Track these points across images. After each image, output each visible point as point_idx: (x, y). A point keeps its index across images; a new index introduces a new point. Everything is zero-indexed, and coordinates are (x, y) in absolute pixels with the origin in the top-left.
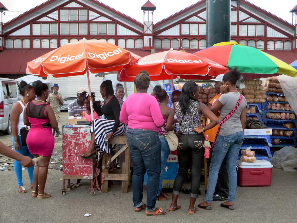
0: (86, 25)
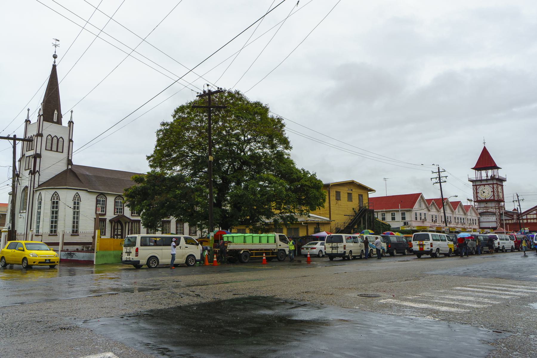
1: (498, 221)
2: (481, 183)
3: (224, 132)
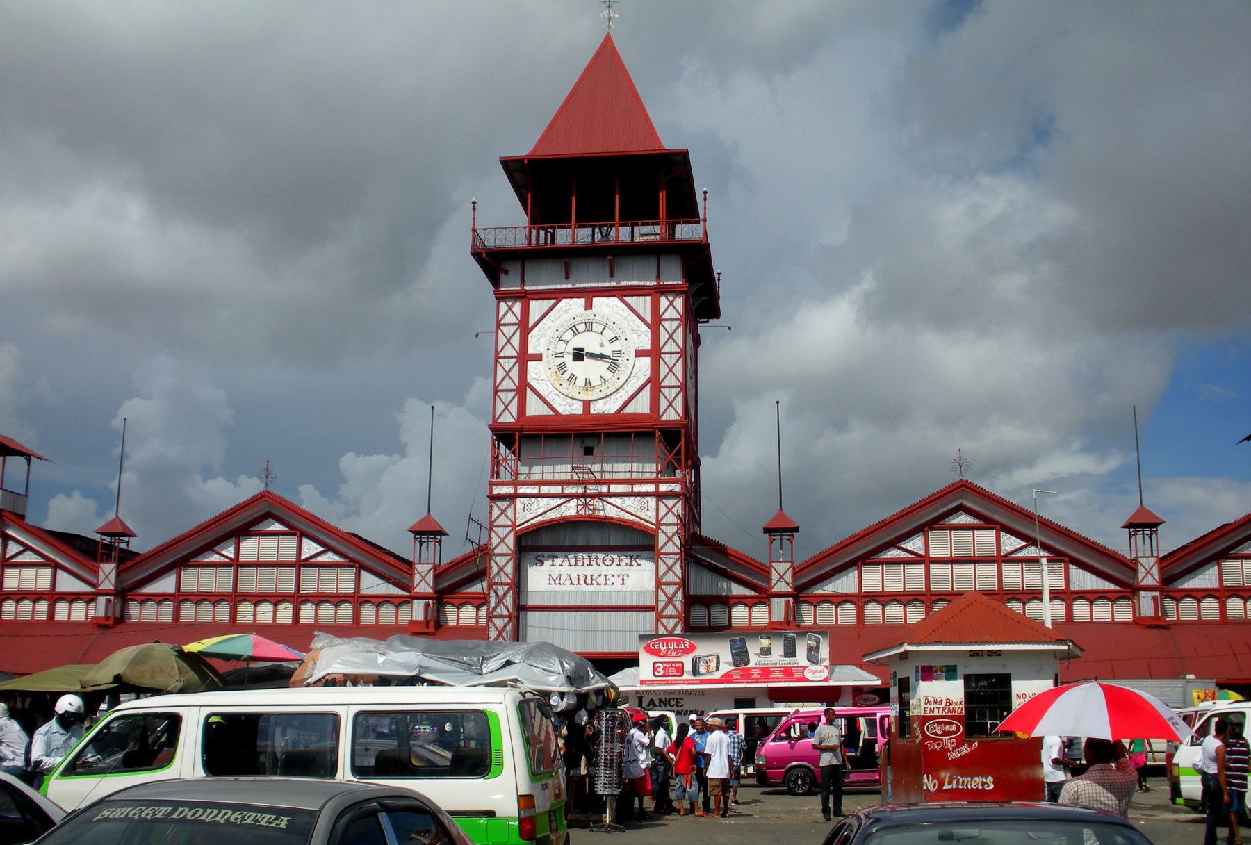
0: (292, 572)
1: (670, 600)
3: (1113, 765)
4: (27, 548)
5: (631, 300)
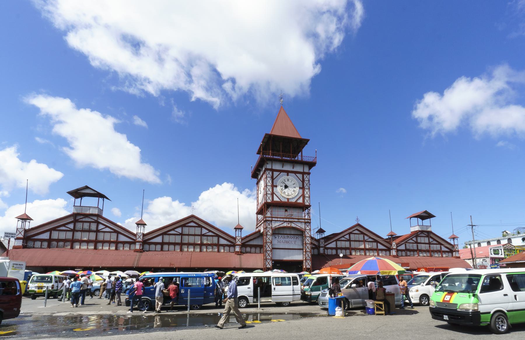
2: (293, 168)
4: (107, 226)
5: (297, 175)
